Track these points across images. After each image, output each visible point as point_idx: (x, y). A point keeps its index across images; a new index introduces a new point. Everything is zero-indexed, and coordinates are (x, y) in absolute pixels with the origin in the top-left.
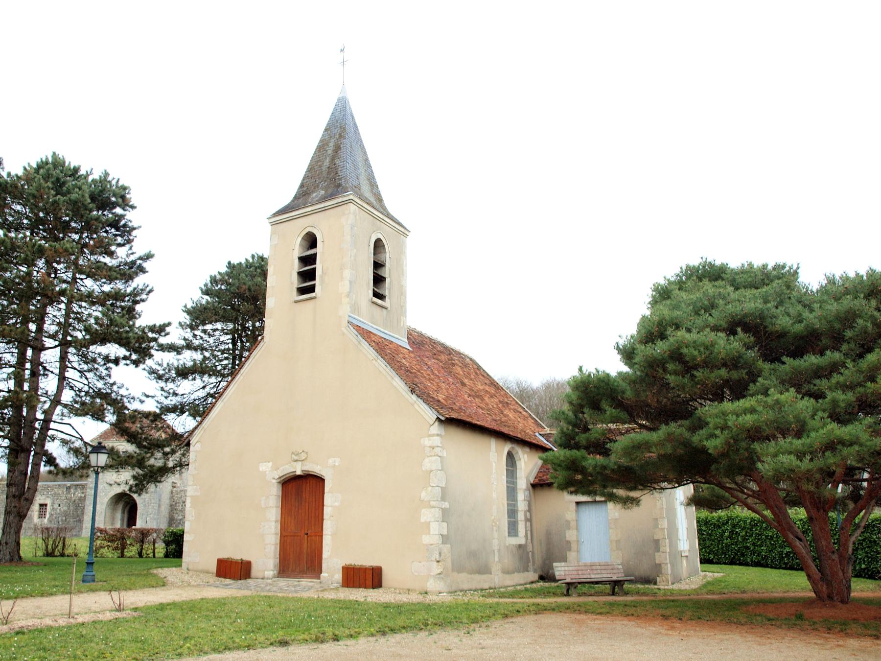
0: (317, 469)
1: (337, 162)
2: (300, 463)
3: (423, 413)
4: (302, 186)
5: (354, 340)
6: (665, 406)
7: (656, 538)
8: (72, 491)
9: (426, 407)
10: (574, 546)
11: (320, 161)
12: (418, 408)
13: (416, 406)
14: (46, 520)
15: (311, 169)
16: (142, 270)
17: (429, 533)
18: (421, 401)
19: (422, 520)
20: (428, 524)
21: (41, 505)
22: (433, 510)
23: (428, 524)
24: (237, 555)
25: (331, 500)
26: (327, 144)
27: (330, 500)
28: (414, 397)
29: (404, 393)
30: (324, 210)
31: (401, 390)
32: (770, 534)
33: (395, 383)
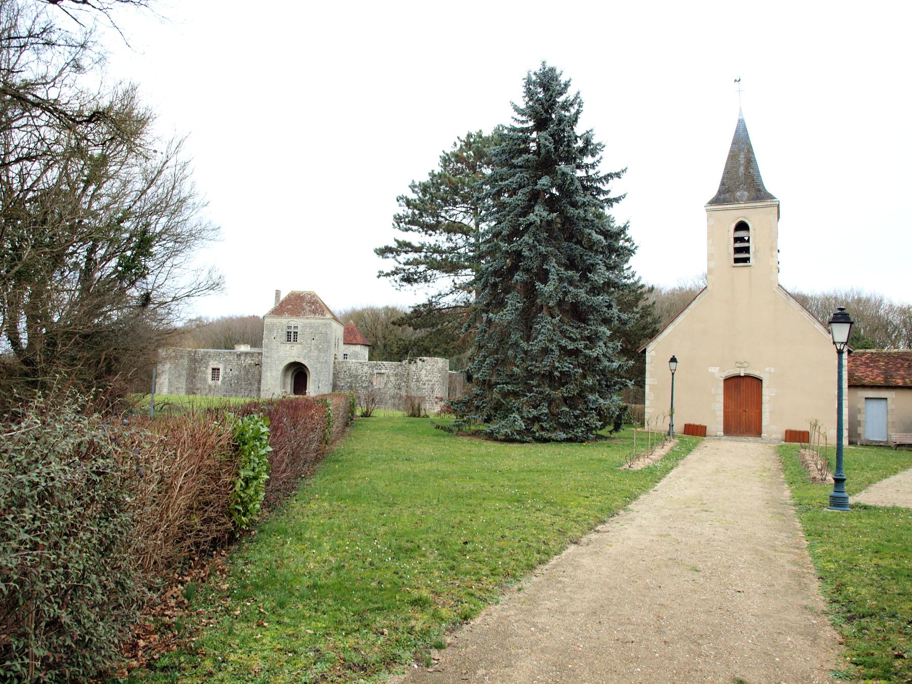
1: (751, 171)
4: (723, 184)
6: (880, 316)
8: (242, 358)
10: (862, 424)
14: (219, 382)
15: (727, 172)
21: (213, 369)
26: (738, 155)
27: (766, 391)
30: (755, 208)
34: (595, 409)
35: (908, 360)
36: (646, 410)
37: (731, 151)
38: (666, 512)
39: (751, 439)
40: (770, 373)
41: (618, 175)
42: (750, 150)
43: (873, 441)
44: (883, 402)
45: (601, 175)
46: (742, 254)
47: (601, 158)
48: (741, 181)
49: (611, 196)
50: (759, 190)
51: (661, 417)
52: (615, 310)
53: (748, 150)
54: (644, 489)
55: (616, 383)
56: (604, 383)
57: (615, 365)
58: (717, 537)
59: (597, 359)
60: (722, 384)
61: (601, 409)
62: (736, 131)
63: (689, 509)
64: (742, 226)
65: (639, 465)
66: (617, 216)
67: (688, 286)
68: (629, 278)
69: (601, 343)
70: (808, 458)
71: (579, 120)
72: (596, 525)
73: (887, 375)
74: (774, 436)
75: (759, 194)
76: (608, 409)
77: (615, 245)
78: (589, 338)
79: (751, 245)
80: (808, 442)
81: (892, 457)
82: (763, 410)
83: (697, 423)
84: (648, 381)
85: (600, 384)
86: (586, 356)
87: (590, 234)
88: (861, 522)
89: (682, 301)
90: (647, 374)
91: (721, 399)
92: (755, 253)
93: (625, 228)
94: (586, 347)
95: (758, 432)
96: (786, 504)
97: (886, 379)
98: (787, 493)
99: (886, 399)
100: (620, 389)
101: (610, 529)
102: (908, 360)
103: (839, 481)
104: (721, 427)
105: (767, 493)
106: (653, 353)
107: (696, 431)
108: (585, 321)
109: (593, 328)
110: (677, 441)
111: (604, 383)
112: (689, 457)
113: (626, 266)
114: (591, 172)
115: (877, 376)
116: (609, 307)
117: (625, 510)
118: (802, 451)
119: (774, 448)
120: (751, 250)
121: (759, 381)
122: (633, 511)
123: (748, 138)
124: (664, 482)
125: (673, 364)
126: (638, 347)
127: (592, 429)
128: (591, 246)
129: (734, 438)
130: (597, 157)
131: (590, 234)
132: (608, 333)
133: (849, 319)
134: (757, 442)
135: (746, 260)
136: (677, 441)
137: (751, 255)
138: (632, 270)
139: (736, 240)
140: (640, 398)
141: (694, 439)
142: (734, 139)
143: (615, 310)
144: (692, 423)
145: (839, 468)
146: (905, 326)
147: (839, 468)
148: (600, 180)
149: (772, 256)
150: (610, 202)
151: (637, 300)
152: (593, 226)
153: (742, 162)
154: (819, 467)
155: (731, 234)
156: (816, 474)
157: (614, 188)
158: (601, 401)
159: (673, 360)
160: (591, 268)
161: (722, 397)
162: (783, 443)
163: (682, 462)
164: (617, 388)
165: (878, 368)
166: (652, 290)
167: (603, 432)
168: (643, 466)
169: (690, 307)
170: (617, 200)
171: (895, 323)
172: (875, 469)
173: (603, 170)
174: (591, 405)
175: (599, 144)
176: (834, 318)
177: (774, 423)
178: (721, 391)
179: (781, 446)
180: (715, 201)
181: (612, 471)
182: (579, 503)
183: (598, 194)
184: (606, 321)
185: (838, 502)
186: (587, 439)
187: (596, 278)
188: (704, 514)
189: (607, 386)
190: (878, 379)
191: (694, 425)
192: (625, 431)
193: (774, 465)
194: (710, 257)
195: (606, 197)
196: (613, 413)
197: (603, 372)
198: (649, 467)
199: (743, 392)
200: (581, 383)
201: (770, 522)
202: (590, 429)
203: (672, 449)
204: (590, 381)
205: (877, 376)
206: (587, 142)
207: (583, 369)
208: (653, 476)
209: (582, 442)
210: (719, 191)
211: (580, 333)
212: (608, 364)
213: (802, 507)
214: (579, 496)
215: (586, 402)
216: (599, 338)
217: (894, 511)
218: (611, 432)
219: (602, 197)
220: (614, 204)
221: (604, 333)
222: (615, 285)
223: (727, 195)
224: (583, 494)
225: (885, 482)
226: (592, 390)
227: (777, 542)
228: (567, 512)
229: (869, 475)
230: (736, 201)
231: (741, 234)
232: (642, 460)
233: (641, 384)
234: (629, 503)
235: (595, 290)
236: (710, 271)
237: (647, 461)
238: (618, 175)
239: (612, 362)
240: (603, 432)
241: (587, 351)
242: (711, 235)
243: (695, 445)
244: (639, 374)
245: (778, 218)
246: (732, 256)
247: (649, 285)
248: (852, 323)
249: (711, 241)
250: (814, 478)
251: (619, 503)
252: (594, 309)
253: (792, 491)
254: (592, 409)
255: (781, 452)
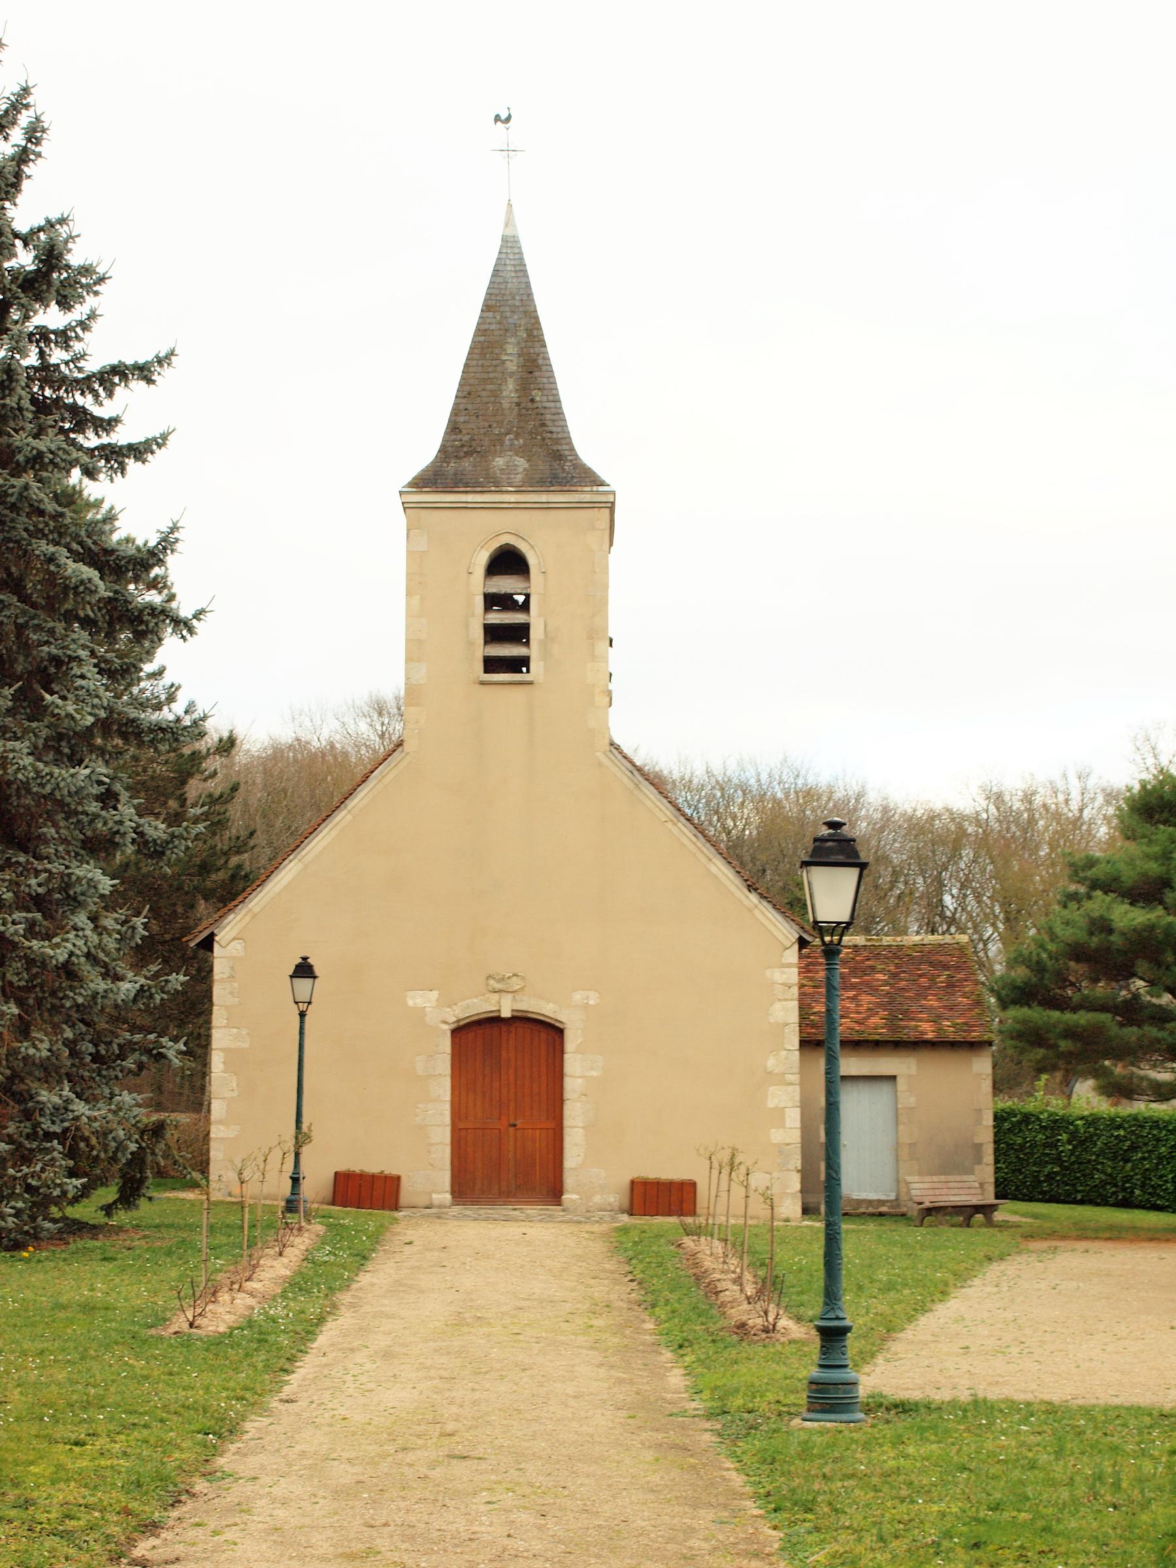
0: (546, 1009)
1: (537, 395)
2: (510, 996)
3: (771, 927)
4: (453, 428)
5: (626, 780)
7: (977, 1140)
9: (779, 917)
11: (490, 381)
12: (760, 917)
13: (756, 912)
16: (160, 562)
17: (783, 1126)
18: (769, 906)
19: (771, 1105)
20: (780, 1112)
22: (791, 1088)
23: (780, 1112)
24: (370, 1162)
25: (579, 1068)
26: (501, 345)
27: (574, 1064)
28: (754, 898)
29: (733, 889)
31: (727, 883)
32: (1019, 1140)
33: (714, 869)
34: (62, 1137)
35: (946, 967)
36: (216, 1132)
37: (480, 331)
38: (343, 1474)
39: (532, 1210)
40: (586, 1007)
41: (144, 372)
42: (533, 335)
43: (859, 1202)
44: (885, 1088)
45: (92, 366)
46: (506, 644)
47: (92, 316)
48: (506, 427)
49: (121, 437)
50: (558, 456)
51: (276, 1156)
52: (127, 810)
53: (530, 333)
54: (252, 1398)
55: (126, 1049)
56: (87, 1047)
57: (127, 988)
58: (521, 1545)
59: (68, 971)
60: (446, 1044)
61: (79, 1137)
62: (496, 273)
63: (410, 1457)
64: (508, 561)
65: (222, 1316)
66: (131, 507)
67: (325, 735)
68: (158, 707)
69: (81, 919)
70: (708, 1263)
71: (25, 185)
72: (131, 1542)
73: (896, 1012)
74: (597, 1199)
75: (558, 469)
76: (105, 1133)
77: (124, 600)
78: (39, 902)
79: (536, 620)
80: (693, 1213)
81: (923, 1247)
82: (567, 1122)
83: (373, 1168)
84: (221, 1037)
85: (74, 1053)
86: (30, 962)
87: (51, 559)
88: (906, 1456)
89: (315, 788)
90: (218, 1017)
91: (443, 1089)
92: (544, 644)
93: (167, 543)
94: (32, 931)
95: (553, 1192)
96: (683, 1413)
97: (892, 1020)
98: (676, 1379)
99: (893, 1078)
100: (141, 1066)
101: (179, 1550)
102: (946, 967)
103: (832, 1335)
104: (444, 1178)
105: (620, 1381)
106: (236, 948)
107: (367, 1193)
108: (27, 843)
109: (56, 867)
110: (318, 1228)
111: (87, 1047)
112: (364, 1279)
113: (148, 668)
114: (57, 356)
115: (871, 1012)
116: (108, 798)
117: (207, 1475)
118: (688, 1242)
119: (604, 1235)
120: (535, 634)
121: (553, 1032)
122: (234, 1477)
123: (530, 295)
124: (306, 1368)
125: (304, 984)
126: (187, 930)
127: (48, 1201)
128: (59, 597)
129: (485, 1211)
130: (79, 312)
131: (51, 559)
132: (106, 884)
133: (856, 854)
134: (551, 1218)
135: (518, 664)
136: (318, 1228)
137: (534, 651)
138: (166, 680)
139: (493, 601)
140: (194, 1091)
141: (371, 1218)
142: (489, 294)
143: (127, 810)
144: (357, 1168)
145: (831, 1295)
146: (923, 872)
147: (831, 1295)
148: (85, 384)
149: (593, 657)
150: (117, 457)
151: (183, 778)
152: (60, 534)
153: (512, 366)
154: (750, 1290)
155: (478, 584)
156: (741, 1312)
157: (132, 412)
158: (80, 1107)
159: (304, 970)
160: (54, 672)
161: (447, 1083)
162: (625, 1218)
163: (345, 1298)
164: (130, 1063)
165: (873, 990)
166: (228, 745)
167: (87, 1211)
168: (230, 1319)
169: (352, 803)
170: (139, 451)
171: (896, 859)
172: (890, 1287)
173: (98, 351)
174: (47, 1125)
175: (86, 270)
176: (816, 851)
177: (598, 1154)
178: (444, 1065)
179: (625, 1230)
180: (428, 481)
181: (137, 1341)
182: (60, 1467)
183: (80, 428)
184: (98, 846)
185: (830, 1398)
186: (35, 1237)
187: (71, 708)
188: (459, 1469)
189: (96, 1058)
190: (874, 1021)
191: (361, 1176)
192: (162, 1202)
193: (620, 1293)
194: (415, 650)
195: (105, 440)
196: (121, 1146)
197: (83, 1014)
198: (250, 1324)
199: (509, 1070)
200: (12, 1053)
201: (655, 1478)
202: (41, 1201)
203: (308, 1258)
204: (40, 1047)
205: (871, 1012)
206: (51, 257)
207: (20, 1003)
208: (270, 1349)
209: (17, 1246)
210: (443, 450)
211: (14, 885)
212: (102, 985)
213: (735, 1420)
214: (53, 1441)
215: (28, 1115)
216: (75, 903)
217: (979, 1412)
218: (108, 1209)
219: (90, 440)
220: (131, 464)
221: (92, 884)
222: (131, 730)
223: (467, 464)
224: (61, 1431)
225: (926, 1323)
226: (49, 1072)
227: (694, 1543)
228: (27, 1504)
229: (883, 1308)
230: (492, 483)
231: (505, 584)
232: (224, 1297)
233: (199, 1048)
234: (216, 1451)
235: (68, 745)
236: (413, 693)
237: (242, 1300)
238: (144, 372)
239: (117, 978)
240: (87, 1211)
241: (35, 944)
242: (416, 582)
243: (376, 1238)
244: (192, 1011)
245: (611, 544)
246: (481, 651)
247: (216, 728)
248: (863, 866)
249: (416, 599)
250: (742, 1325)
251: (186, 1454)
252: (60, 806)
253: (689, 1372)
254: (49, 1136)
255: (632, 1255)
